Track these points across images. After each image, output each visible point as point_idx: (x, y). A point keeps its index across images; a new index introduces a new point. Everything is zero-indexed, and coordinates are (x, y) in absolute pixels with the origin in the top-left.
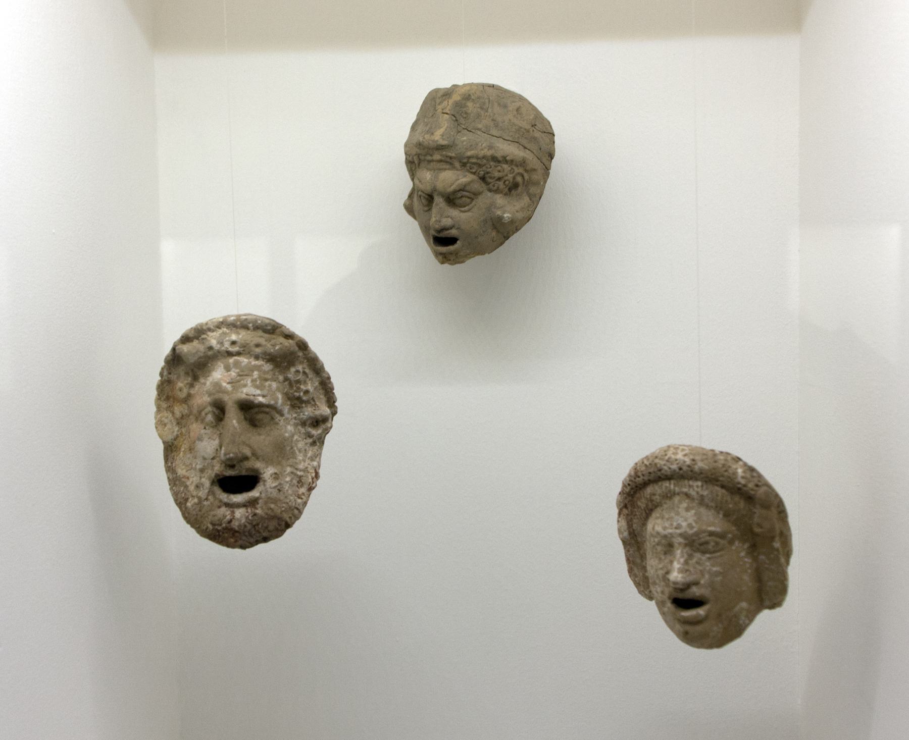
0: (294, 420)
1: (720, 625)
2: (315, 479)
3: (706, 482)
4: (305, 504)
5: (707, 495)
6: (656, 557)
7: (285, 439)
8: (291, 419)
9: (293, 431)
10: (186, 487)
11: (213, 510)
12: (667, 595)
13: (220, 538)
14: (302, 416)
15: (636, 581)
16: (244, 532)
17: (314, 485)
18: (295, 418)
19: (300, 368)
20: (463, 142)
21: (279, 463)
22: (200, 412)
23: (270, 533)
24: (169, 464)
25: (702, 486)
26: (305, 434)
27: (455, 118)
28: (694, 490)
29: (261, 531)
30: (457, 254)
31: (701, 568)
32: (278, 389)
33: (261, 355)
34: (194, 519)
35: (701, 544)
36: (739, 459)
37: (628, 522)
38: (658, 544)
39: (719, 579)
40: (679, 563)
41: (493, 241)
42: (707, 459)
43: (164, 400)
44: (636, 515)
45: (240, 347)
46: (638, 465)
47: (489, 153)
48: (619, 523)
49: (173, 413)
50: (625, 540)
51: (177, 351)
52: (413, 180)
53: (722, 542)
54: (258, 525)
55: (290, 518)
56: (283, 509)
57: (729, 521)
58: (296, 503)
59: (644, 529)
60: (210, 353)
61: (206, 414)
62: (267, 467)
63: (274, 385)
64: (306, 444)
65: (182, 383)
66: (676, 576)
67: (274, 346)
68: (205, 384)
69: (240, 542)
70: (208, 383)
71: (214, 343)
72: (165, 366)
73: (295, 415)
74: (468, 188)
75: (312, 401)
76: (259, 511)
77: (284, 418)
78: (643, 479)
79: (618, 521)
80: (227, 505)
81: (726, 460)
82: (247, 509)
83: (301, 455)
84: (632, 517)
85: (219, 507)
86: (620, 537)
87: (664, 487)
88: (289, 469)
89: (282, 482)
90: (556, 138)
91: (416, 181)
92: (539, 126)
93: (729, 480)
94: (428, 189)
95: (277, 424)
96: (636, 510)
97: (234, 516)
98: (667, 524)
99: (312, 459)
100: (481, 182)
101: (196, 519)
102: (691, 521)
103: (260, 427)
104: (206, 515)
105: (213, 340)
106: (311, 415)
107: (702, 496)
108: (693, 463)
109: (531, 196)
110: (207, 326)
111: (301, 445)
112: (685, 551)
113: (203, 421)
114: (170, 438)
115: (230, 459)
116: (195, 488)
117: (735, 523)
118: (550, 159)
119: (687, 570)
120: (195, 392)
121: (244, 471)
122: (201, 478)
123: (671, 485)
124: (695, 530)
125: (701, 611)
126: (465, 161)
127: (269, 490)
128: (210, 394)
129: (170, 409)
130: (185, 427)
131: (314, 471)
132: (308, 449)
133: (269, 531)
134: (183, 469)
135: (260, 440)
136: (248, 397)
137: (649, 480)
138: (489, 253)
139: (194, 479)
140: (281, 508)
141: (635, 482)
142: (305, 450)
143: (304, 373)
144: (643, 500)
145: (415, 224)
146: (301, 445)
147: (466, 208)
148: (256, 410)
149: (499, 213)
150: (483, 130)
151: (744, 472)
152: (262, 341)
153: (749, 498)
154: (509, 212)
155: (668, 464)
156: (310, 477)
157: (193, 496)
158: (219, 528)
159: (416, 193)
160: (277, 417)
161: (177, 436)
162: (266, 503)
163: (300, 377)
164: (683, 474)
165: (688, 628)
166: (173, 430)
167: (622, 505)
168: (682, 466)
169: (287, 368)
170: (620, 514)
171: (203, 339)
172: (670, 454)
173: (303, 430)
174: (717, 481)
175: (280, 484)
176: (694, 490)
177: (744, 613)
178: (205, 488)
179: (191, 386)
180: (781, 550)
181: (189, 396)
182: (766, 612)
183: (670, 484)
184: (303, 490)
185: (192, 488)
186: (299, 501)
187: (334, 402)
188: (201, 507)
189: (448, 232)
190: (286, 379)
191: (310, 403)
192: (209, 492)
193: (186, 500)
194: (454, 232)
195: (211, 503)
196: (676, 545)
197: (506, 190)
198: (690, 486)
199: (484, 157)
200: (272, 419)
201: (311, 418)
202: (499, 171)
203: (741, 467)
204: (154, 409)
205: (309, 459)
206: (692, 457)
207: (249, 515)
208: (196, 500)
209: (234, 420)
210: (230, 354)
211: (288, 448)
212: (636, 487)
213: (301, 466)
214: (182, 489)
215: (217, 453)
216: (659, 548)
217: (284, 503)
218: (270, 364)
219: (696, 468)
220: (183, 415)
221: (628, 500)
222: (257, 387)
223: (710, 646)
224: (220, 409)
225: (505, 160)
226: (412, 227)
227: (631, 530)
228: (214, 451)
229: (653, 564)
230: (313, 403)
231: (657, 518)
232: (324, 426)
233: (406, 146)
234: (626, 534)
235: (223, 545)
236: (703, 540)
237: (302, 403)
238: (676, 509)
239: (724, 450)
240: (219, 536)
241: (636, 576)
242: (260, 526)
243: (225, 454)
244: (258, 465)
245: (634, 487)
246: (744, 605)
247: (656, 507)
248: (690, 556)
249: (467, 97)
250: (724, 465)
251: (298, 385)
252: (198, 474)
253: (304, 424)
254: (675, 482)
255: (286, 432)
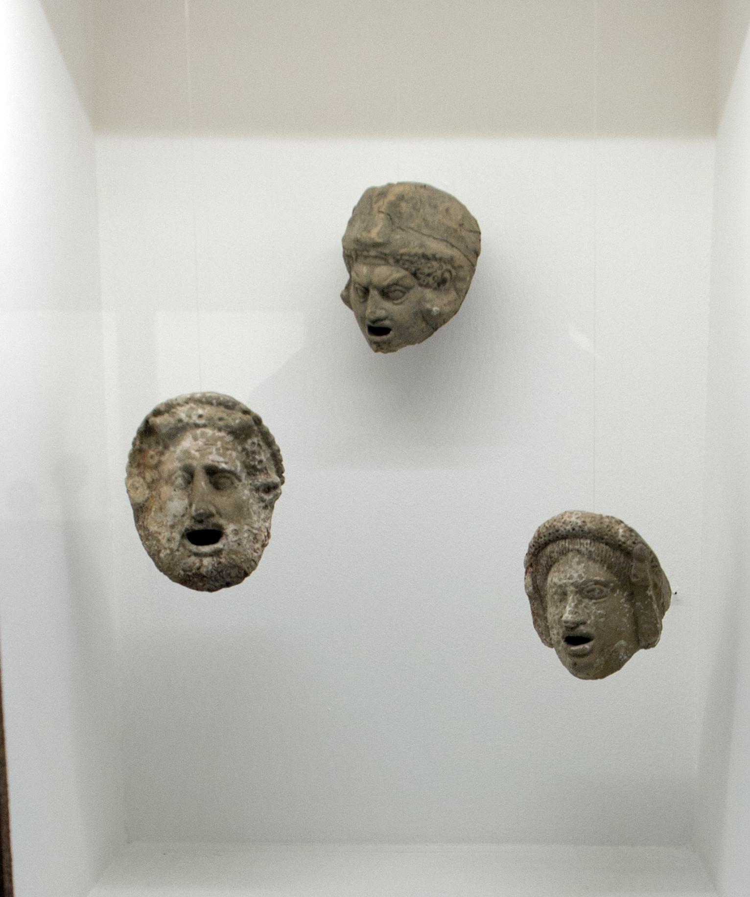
0: (249, 486)
1: (602, 658)
2: (267, 538)
3: (594, 540)
4: (260, 557)
5: (594, 551)
6: (554, 605)
7: (244, 502)
8: (248, 485)
9: (249, 495)
10: (158, 541)
11: (184, 559)
12: (561, 635)
13: (191, 582)
14: (256, 482)
15: (539, 631)
16: (211, 577)
17: (266, 543)
18: (251, 484)
19: (255, 440)
20: (397, 240)
21: (238, 522)
22: (170, 476)
23: (232, 579)
24: (141, 523)
25: (591, 543)
26: (259, 499)
27: (390, 217)
28: (584, 546)
29: (225, 577)
30: (390, 343)
31: (588, 611)
32: (237, 458)
33: (223, 428)
34: (167, 568)
35: (588, 592)
36: (622, 522)
37: (532, 579)
38: (555, 594)
39: (602, 620)
40: (570, 606)
41: (423, 332)
42: (595, 521)
43: (136, 467)
44: (539, 572)
45: (206, 420)
46: (541, 528)
47: (420, 251)
48: (526, 580)
49: (144, 478)
50: (530, 595)
51: (150, 423)
52: (350, 272)
53: (605, 589)
54: (222, 571)
55: (248, 568)
56: (243, 560)
57: (612, 573)
58: (252, 556)
59: (545, 584)
60: (180, 425)
61: (176, 478)
62: (229, 524)
63: (234, 454)
64: (260, 507)
65: (153, 451)
66: (567, 616)
67: (234, 420)
68: (175, 452)
69: (207, 586)
70: (178, 451)
71: (183, 416)
72: (137, 437)
73: (250, 482)
74: (400, 283)
75: (264, 470)
76: (223, 560)
77: (241, 483)
78: (545, 540)
79: (525, 579)
80: (197, 554)
81: (610, 522)
82: (213, 558)
83: (256, 516)
84: (536, 574)
85: (189, 556)
86: (526, 592)
87: (560, 546)
88: (246, 528)
89: (241, 537)
90: (482, 236)
91: (353, 274)
92: (467, 226)
93: (612, 538)
94: (364, 281)
95: (236, 488)
96: (539, 567)
97: (202, 564)
98: (562, 576)
99: (265, 520)
100: (413, 278)
101: (169, 567)
102: (580, 572)
103: (222, 490)
104: (178, 563)
105: (182, 413)
106: (265, 482)
107: (590, 551)
108: (584, 524)
109: (458, 291)
110: (177, 402)
111: (255, 507)
112: (575, 597)
113: (172, 484)
114: (140, 499)
115: (200, 515)
116: (167, 542)
117: (616, 575)
118: (475, 256)
119: (576, 613)
120: (165, 459)
121: (210, 526)
122: (171, 533)
123: (566, 544)
124: (584, 579)
125: (587, 646)
126: (399, 257)
127: (231, 543)
128: (180, 460)
129: (141, 475)
130: (155, 490)
131: (266, 531)
132: (261, 512)
133: (231, 578)
134: (154, 526)
135: (223, 501)
136: (214, 463)
137: (550, 541)
138: (419, 343)
139: (164, 535)
140: (240, 559)
141: (539, 543)
142: (259, 512)
143: (259, 445)
144: (545, 558)
145: (351, 314)
146: (255, 507)
147: (399, 301)
148: (219, 475)
149: (428, 306)
150: (415, 229)
151: (624, 532)
152: (224, 415)
153: (628, 554)
154: (437, 306)
155: (564, 526)
156: (263, 536)
157: (165, 548)
158: (190, 574)
159: (352, 285)
160: (236, 482)
161: (148, 498)
162: (228, 554)
163: (256, 448)
164: (576, 534)
165: (576, 660)
166: (142, 494)
167: (528, 564)
168: (575, 527)
169: (245, 440)
170: (526, 572)
171: (173, 413)
172: (566, 517)
173: (257, 495)
174: (603, 539)
175: (240, 539)
176: (584, 546)
177: (623, 650)
178: (176, 541)
179: (162, 454)
180: (654, 598)
181: (160, 463)
182: (642, 651)
183: (565, 542)
184: (258, 546)
185: (164, 541)
186: (255, 554)
187: (283, 472)
188: (172, 557)
189: (382, 323)
190: (244, 449)
191: (263, 472)
192: (179, 544)
193: (159, 552)
194: (387, 323)
195: (182, 553)
196: (569, 592)
197: (435, 285)
198: (581, 544)
199: (416, 255)
200: (232, 483)
201: (265, 485)
202: (429, 268)
203: (622, 528)
204: (125, 475)
205: (262, 520)
206: (583, 519)
207: (215, 563)
208: (168, 551)
209: (202, 483)
210: (197, 426)
211: (246, 509)
212: (539, 547)
213: (256, 525)
214: (155, 542)
215: (187, 511)
216: (556, 597)
217: (243, 555)
218: (231, 436)
219: (586, 528)
220: (153, 480)
221: (533, 559)
222: (221, 455)
223: (595, 677)
224: (189, 474)
225: (434, 258)
226: (348, 316)
227: (535, 585)
228: (184, 509)
229: (551, 610)
230: (265, 472)
231: (555, 572)
232: (275, 492)
233: (344, 240)
234: (531, 588)
235: (193, 589)
236: (590, 588)
237: (256, 472)
238: (569, 562)
239: (610, 515)
240: (190, 580)
241: (539, 626)
242: (224, 573)
243: (196, 510)
244: (222, 522)
245: (537, 547)
246: (623, 642)
247: (554, 563)
248: (580, 602)
249: (401, 198)
250: (608, 526)
251: (254, 455)
252: (169, 530)
253: (257, 490)
254: (570, 541)
255: (244, 495)
